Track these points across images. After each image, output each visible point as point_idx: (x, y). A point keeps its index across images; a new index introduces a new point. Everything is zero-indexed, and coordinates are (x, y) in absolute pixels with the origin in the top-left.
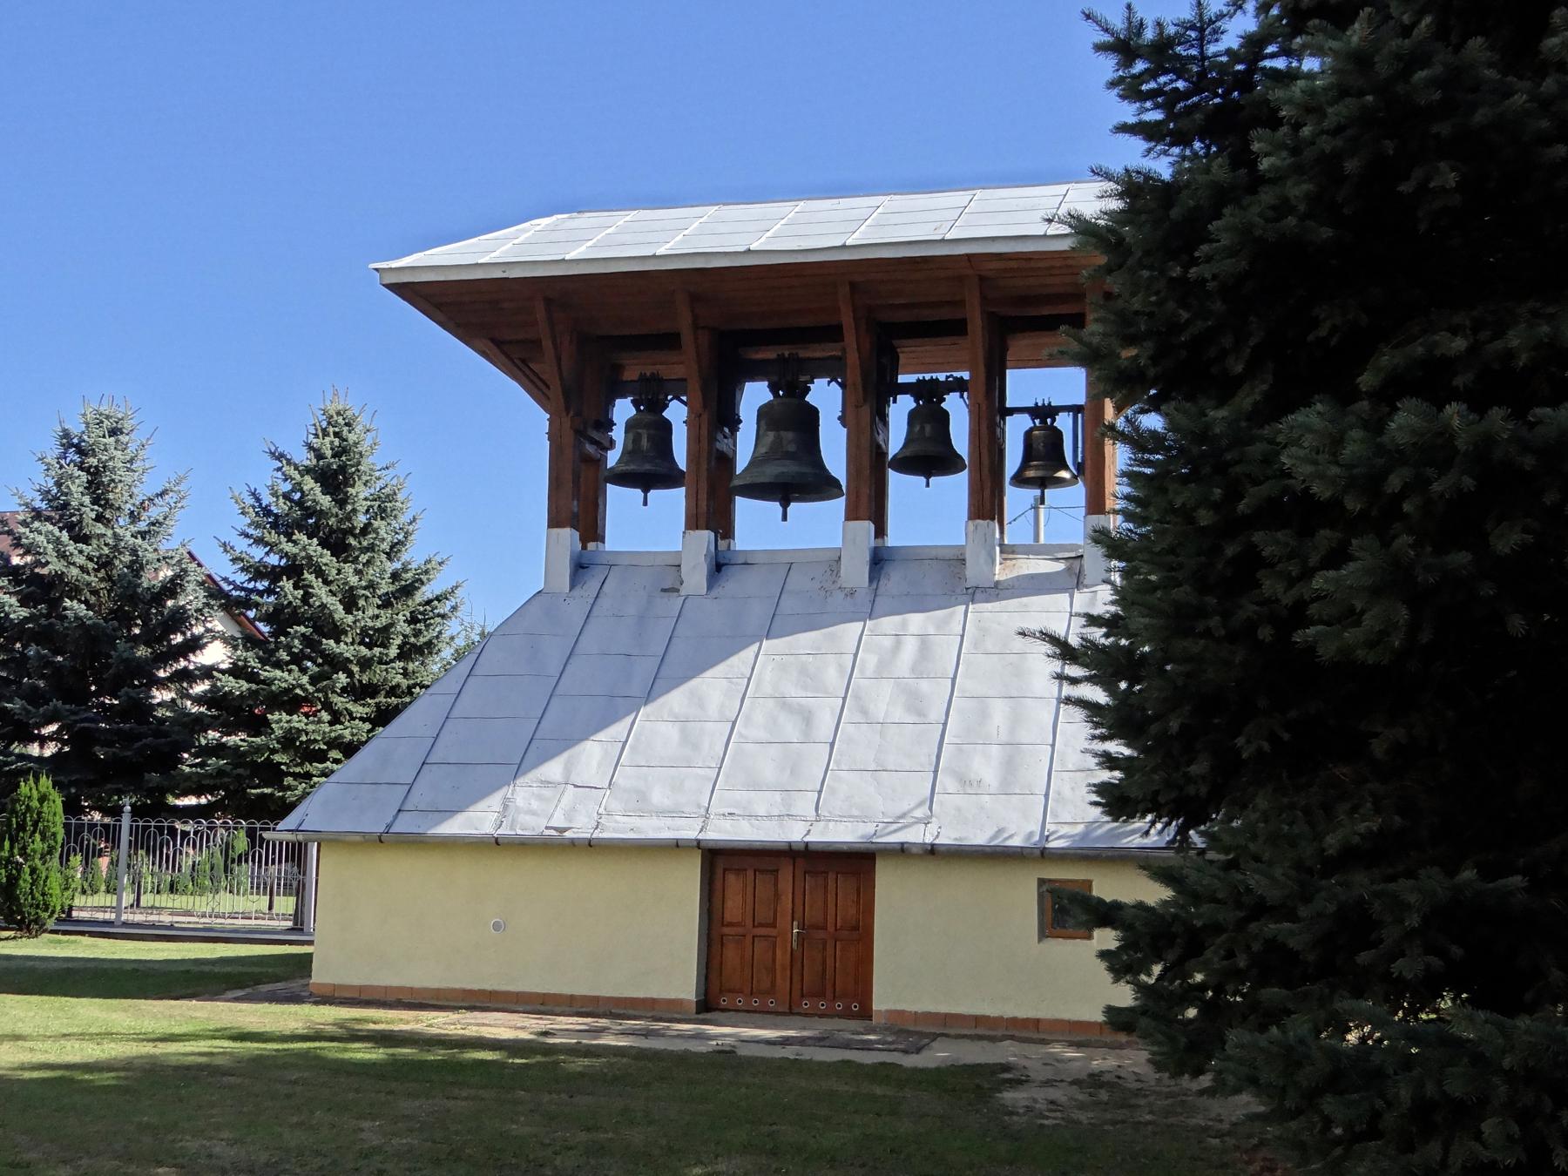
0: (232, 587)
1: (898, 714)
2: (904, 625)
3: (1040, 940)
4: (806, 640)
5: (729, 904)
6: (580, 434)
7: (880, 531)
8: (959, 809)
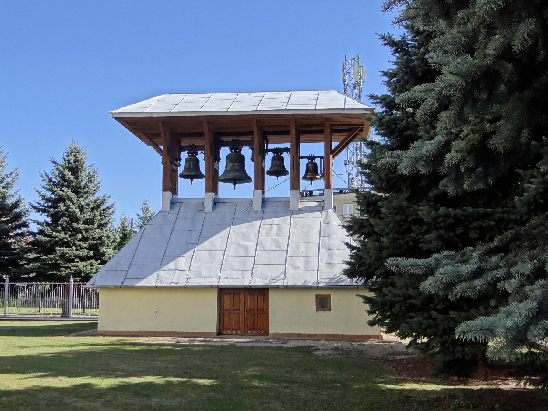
0: (40, 205)
1: (273, 248)
2: (273, 221)
3: (316, 312)
4: (244, 226)
5: (226, 304)
6: (172, 163)
7: (263, 193)
8: (293, 275)
